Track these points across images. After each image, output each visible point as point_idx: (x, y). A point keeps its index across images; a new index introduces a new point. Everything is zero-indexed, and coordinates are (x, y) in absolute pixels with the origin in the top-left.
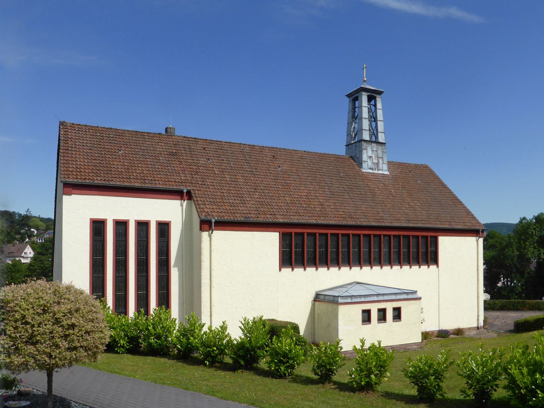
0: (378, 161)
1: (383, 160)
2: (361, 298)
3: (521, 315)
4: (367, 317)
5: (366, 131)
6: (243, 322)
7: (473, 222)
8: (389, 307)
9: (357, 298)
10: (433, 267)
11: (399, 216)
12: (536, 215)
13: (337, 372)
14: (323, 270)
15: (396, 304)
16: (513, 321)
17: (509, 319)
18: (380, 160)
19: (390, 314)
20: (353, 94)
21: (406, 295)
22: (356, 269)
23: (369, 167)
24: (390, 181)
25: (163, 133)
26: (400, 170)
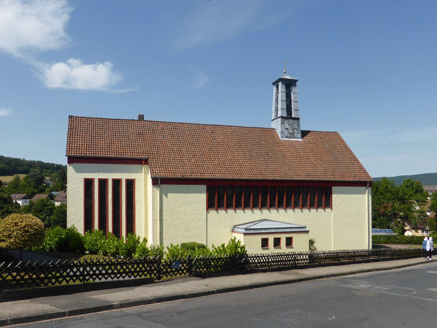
0: (294, 131)
1: (297, 131)
2: (254, 231)
3: (408, 247)
4: (265, 243)
5: (284, 110)
10: (328, 210)
14: (239, 212)
18: (295, 131)
20: (276, 82)
21: (253, 230)
22: (265, 212)
23: (286, 136)
25: (135, 119)
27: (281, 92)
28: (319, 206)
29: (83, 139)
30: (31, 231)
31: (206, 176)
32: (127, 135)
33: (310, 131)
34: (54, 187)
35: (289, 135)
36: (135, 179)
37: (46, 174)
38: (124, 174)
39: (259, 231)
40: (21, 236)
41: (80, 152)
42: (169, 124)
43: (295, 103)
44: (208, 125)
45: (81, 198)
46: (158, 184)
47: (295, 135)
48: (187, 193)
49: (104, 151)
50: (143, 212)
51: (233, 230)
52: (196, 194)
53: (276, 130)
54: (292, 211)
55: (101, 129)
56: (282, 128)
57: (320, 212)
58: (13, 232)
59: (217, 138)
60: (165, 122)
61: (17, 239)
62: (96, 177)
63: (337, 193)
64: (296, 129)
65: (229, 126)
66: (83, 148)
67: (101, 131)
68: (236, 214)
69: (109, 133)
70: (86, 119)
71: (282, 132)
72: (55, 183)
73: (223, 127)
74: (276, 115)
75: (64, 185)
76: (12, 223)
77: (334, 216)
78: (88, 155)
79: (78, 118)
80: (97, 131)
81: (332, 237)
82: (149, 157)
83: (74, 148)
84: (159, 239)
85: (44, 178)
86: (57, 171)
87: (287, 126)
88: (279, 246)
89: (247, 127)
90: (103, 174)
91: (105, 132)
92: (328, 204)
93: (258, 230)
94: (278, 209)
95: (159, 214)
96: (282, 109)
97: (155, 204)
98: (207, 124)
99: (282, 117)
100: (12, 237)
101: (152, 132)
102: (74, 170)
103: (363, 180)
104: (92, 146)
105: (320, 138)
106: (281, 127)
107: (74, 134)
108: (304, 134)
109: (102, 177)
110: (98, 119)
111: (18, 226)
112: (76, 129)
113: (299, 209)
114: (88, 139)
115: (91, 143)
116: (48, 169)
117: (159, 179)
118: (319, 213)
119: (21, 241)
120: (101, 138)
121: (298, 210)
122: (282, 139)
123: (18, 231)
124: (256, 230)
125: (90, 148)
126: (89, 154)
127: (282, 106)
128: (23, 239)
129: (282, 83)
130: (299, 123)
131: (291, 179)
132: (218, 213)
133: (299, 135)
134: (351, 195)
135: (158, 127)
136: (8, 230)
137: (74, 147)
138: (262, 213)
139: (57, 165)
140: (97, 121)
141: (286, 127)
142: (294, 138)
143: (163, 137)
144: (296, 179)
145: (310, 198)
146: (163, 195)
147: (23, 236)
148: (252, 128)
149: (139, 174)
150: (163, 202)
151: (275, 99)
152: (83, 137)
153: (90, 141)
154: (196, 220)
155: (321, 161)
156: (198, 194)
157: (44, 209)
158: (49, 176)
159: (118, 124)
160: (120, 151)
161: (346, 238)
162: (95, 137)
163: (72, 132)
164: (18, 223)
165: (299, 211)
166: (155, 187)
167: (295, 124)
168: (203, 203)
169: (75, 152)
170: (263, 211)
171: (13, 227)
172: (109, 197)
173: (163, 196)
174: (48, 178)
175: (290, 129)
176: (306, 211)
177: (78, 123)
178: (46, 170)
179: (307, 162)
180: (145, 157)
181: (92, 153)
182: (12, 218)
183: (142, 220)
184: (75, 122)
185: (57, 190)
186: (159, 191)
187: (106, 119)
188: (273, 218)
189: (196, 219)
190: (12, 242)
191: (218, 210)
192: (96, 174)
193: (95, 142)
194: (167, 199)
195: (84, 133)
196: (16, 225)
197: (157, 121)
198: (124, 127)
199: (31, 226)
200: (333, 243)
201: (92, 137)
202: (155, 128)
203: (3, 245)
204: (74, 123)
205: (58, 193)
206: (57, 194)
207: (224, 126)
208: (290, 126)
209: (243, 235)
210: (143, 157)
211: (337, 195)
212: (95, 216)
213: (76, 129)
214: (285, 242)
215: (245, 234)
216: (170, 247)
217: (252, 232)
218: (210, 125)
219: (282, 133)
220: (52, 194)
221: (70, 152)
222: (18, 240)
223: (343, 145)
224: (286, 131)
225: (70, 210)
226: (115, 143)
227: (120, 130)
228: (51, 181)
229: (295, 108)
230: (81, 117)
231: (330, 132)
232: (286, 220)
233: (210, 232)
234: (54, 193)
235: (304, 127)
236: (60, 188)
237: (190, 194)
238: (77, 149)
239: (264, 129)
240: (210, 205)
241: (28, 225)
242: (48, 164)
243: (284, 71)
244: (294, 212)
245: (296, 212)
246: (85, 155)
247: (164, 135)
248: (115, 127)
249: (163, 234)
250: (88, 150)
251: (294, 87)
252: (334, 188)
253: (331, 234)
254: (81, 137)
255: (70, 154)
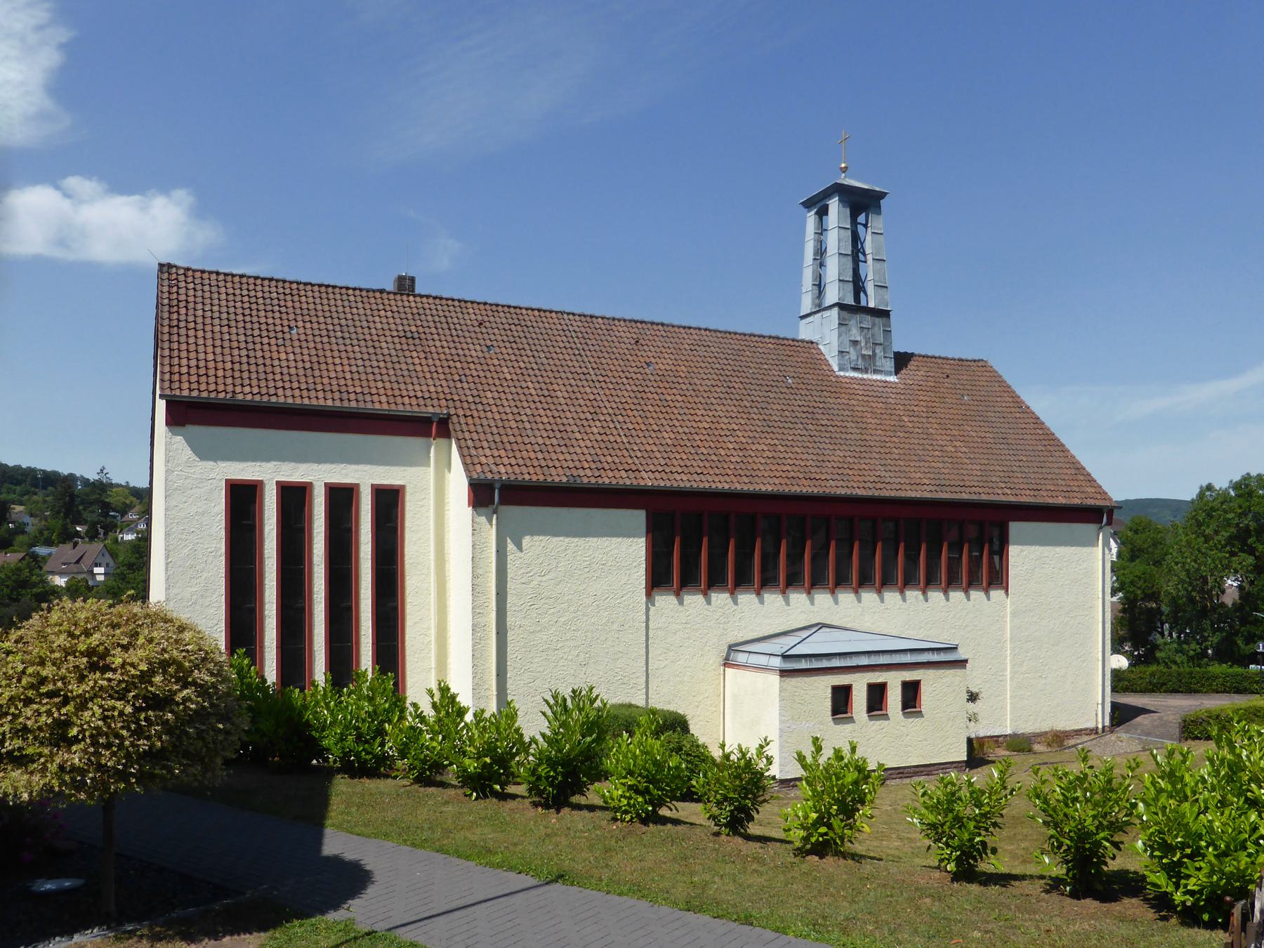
0: (874, 351)
6: (552, 702)
7: (1089, 490)
8: (894, 682)
9: (830, 660)
10: (997, 594)
11: (919, 475)
12: (1237, 478)
13: (758, 812)
14: (747, 599)
15: (910, 676)
16: (1178, 716)
17: (1169, 712)
18: (879, 350)
19: (894, 697)
21: (806, 661)
22: (823, 598)
23: (852, 366)
24: (898, 397)
25: (388, 289)
26: (922, 373)
27: (839, 227)
28: (972, 582)
29: (218, 343)
30: (185, 700)
31: (648, 480)
32: (368, 337)
33: (912, 355)
34: (41, 533)
35: (861, 364)
36: (403, 487)
37: (12, 496)
38: (368, 467)
39: (825, 664)
40: (129, 729)
41: (212, 387)
42: (500, 309)
43: (878, 265)
44: (619, 320)
45: (217, 550)
46: (494, 504)
47: (877, 364)
48: (586, 537)
49: (295, 385)
50: (432, 600)
51: (727, 659)
52: (614, 540)
53: (820, 347)
54: (897, 595)
55: (277, 315)
56: (842, 338)
57: (975, 601)
58: (83, 705)
59: (653, 361)
60: (485, 304)
61: (108, 746)
62: (268, 476)
63: (1021, 542)
64: (881, 344)
65: (684, 328)
66: (220, 373)
67: (278, 322)
68: (735, 607)
69: (233, 369)
70: (221, 277)
71: (841, 352)
72: (43, 522)
73: (667, 329)
74: (817, 301)
75: (69, 527)
76: (68, 652)
77: (1014, 614)
78: (240, 397)
79: (190, 273)
80: (263, 320)
81: (1008, 677)
82: (452, 411)
83: (188, 373)
84: (495, 693)
85: (9, 508)
86: (44, 488)
87: (855, 334)
88: (881, 710)
89: (735, 334)
90: (293, 465)
91: (293, 324)
92: (997, 578)
93: (822, 660)
94: (860, 590)
95: (494, 609)
96: (840, 280)
97: (480, 571)
98: (617, 317)
99: (842, 306)
100: (76, 740)
101: (447, 332)
102: (189, 452)
103: (1090, 502)
104: (253, 368)
105: (945, 376)
106: (840, 336)
107: (182, 324)
108: (902, 361)
109: (291, 475)
110: (263, 279)
111: (107, 668)
112: (187, 309)
113: (918, 590)
114: (235, 344)
115: (248, 356)
116: (18, 483)
117: (497, 485)
118: (971, 603)
119: (128, 756)
120: (280, 342)
121: (913, 595)
122: (842, 373)
123: (111, 703)
124: (817, 660)
125: (246, 375)
126: (245, 394)
127: (841, 271)
128: (143, 744)
129: (840, 201)
130: (890, 326)
131: (893, 494)
132: (681, 603)
133: (889, 365)
134: (1059, 549)
135: (467, 317)
136: (51, 695)
137: (189, 367)
138: (812, 603)
139: (44, 471)
140: (259, 288)
141: (853, 339)
142: (876, 372)
143: (485, 349)
144: (913, 494)
145: (927, 555)
146: (509, 541)
147: (139, 733)
148: (750, 335)
149: (423, 468)
150: (509, 566)
151: (814, 250)
152: (218, 336)
153: (244, 352)
154: (615, 627)
155: (967, 444)
156: (620, 540)
157: (21, 595)
158: (21, 504)
159: (332, 302)
160: (351, 389)
161: (1044, 681)
162: (258, 340)
163: (175, 316)
164: (103, 656)
165: (916, 597)
166: (479, 515)
167: (876, 329)
168: (636, 570)
169: (195, 386)
170: (816, 596)
171: (82, 679)
172: (315, 546)
173: (506, 547)
174: (19, 508)
175: (863, 344)
176: (936, 596)
177: (195, 289)
178: (13, 487)
179: (927, 447)
180: (438, 410)
181: (256, 390)
182: (65, 626)
183: (429, 629)
184: (182, 284)
185: (49, 543)
186: (494, 527)
187: (291, 283)
188: (845, 620)
189: (613, 623)
190: (74, 769)
191: (762, 592)
192: (271, 465)
193: (259, 354)
194: (521, 555)
195: (217, 322)
196: (93, 667)
197: (461, 297)
198: (355, 311)
199: (180, 666)
200: (1008, 696)
201: (250, 339)
202: (456, 320)
203: (16, 789)
204: (179, 288)
205: (53, 550)
206: (50, 555)
207: (668, 326)
208: (863, 333)
209: (775, 679)
210: (430, 409)
211: (1020, 547)
212: (266, 613)
213: (187, 309)
214: (899, 698)
215: (784, 673)
216: (808, 751)
217: (804, 665)
218: (625, 320)
219: (843, 357)
220: (34, 552)
221: (176, 385)
222: (114, 754)
223: (1011, 400)
224: (852, 349)
225: (177, 594)
226: (330, 360)
227: (343, 322)
228: (32, 515)
229: (877, 278)
230: (203, 272)
231: (967, 361)
232: (883, 627)
233: (656, 667)
234: (42, 550)
235: (900, 346)
236: (59, 535)
237: (595, 539)
238: (199, 376)
239: (786, 342)
240: (658, 579)
241: (164, 665)
242: (18, 468)
243: (843, 165)
244: (904, 600)
245: (908, 602)
246: (229, 396)
247: (489, 343)
248: (224, 369)
249: (508, 675)
250: (238, 382)
251: (874, 215)
252: (1015, 528)
253: (1005, 670)
254: (209, 335)
255: (177, 392)
